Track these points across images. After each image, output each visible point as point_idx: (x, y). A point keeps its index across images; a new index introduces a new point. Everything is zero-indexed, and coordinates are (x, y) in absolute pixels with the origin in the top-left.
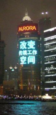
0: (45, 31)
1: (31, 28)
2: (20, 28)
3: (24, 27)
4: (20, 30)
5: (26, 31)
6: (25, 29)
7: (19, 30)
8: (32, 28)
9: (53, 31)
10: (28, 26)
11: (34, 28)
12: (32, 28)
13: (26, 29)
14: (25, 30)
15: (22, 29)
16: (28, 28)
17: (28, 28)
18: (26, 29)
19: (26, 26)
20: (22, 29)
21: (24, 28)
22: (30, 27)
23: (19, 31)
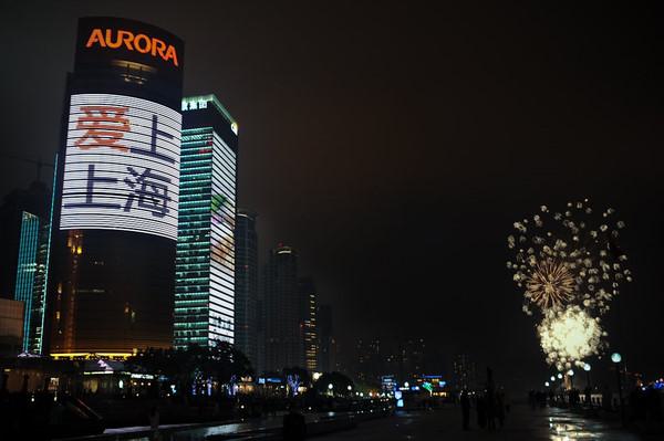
2: (97, 32)
5: (134, 56)
6: (127, 42)
7: (92, 39)
8: (165, 53)
10: (142, 36)
12: (165, 53)
13: (132, 43)
14: (130, 47)
15: (114, 40)
16: (143, 44)
17: (143, 44)
18: (132, 43)
20: (114, 40)
21: (126, 37)
22: (155, 40)
23: (89, 45)
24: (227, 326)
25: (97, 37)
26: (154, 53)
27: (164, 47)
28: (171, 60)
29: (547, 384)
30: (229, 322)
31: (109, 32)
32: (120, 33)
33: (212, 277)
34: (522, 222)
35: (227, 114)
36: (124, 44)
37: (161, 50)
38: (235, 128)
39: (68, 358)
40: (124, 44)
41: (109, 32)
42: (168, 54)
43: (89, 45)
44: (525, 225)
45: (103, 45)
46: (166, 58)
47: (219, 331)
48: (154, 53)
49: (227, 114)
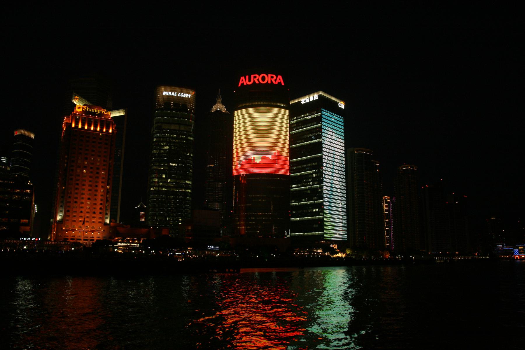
2: (243, 78)
3: (252, 76)
4: (243, 84)
7: (241, 82)
8: (275, 80)
9: (66, 128)
10: (263, 83)
11: (278, 81)
12: (275, 80)
13: (258, 80)
14: (257, 82)
15: (250, 81)
16: (263, 79)
17: (263, 79)
18: (258, 80)
20: (250, 81)
21: (255, 77)
22: (270, 75)
23: (239, 86)
24: (327, 169)
26: (269, 82)
27: (275, 78)
28: (280, 83)
30: (325, 170)
31: (247, 77)
34: (401, 256)
35: (333, 99)
36: (254, 81)
37: (273, 80)
38: (342, 105)
40: (254, 81)
41: (247, 77)
43: (239, 86)
44: (401, 258)
45: (245, 84)
46: (335, 248)
48: (269, 82)
49: (333, 99)
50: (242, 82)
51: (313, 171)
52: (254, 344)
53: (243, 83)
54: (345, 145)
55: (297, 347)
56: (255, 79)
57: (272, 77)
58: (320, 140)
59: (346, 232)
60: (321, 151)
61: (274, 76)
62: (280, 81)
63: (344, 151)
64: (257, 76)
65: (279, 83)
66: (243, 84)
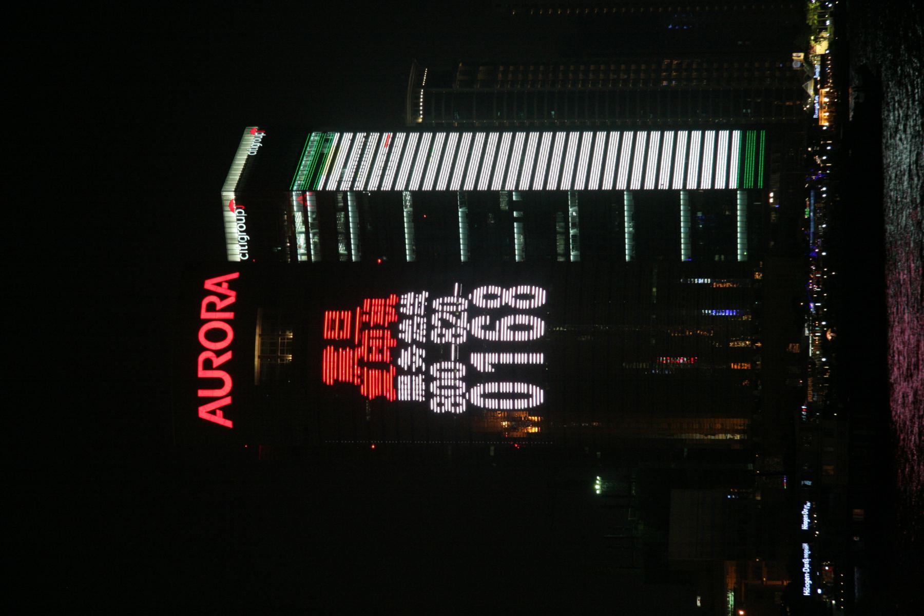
0: (760, 203)
1: (220, 305)
2: (203, 412)
4: (227, 411)
5: (242, 347)
6: (217, 362)
7: (219, 419)
8: (223, 297)
11: (224, 289)
12: (223, 297)
13: (219, 353)
14: (228, 356)
15: (219, 383)
16: (216, 335)
17: (216, 335)
18: (219, 353)
19: (448, 413)
20: (219, 383)
21: (208, 364)
22: (204, 315)
23: (229, 424)
25: (213, 412)
26: (230, 315)
28: (232, 285)
29: (385, 258)
31: (202, 393)
32: (202, 373)
33: (345, 186)
39: (629, 233)
41: (202, 393)
42: (224, 289)
43: (229, 424)
45: (228, 401)
47: (360, 186)
48: (230, 315)
50: (219, 413)
51: (516, 230)
52: (897, 378)
53: (224, 410)
54: (361, 131)
55: (492, 370)
56: (215, 366)
57: (211, 307)
58: (408, 197)
59: (666, 187)
60: (394, 197)
61: (206, 301)
62: (225, 285)
63: (385, 135)
64: (203, 356)
65: (230, 288)
66: (227, 411)
